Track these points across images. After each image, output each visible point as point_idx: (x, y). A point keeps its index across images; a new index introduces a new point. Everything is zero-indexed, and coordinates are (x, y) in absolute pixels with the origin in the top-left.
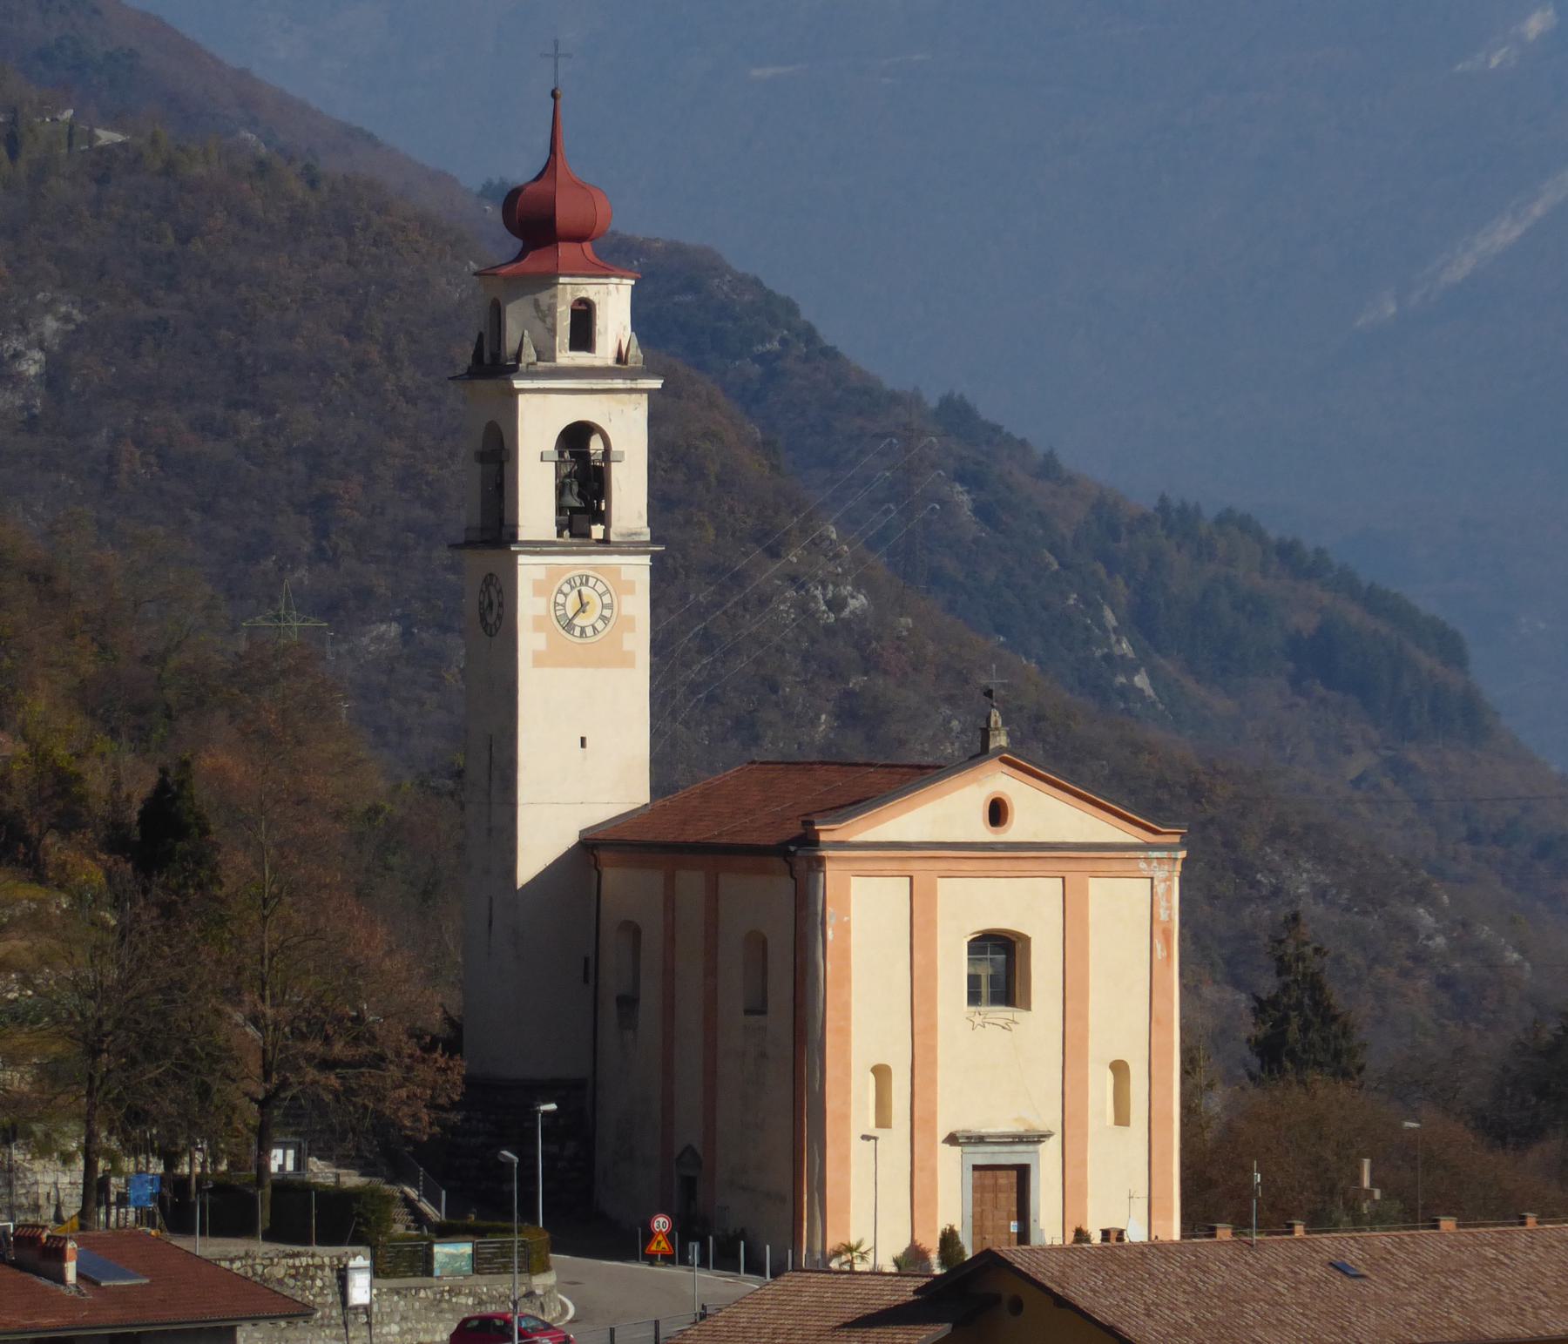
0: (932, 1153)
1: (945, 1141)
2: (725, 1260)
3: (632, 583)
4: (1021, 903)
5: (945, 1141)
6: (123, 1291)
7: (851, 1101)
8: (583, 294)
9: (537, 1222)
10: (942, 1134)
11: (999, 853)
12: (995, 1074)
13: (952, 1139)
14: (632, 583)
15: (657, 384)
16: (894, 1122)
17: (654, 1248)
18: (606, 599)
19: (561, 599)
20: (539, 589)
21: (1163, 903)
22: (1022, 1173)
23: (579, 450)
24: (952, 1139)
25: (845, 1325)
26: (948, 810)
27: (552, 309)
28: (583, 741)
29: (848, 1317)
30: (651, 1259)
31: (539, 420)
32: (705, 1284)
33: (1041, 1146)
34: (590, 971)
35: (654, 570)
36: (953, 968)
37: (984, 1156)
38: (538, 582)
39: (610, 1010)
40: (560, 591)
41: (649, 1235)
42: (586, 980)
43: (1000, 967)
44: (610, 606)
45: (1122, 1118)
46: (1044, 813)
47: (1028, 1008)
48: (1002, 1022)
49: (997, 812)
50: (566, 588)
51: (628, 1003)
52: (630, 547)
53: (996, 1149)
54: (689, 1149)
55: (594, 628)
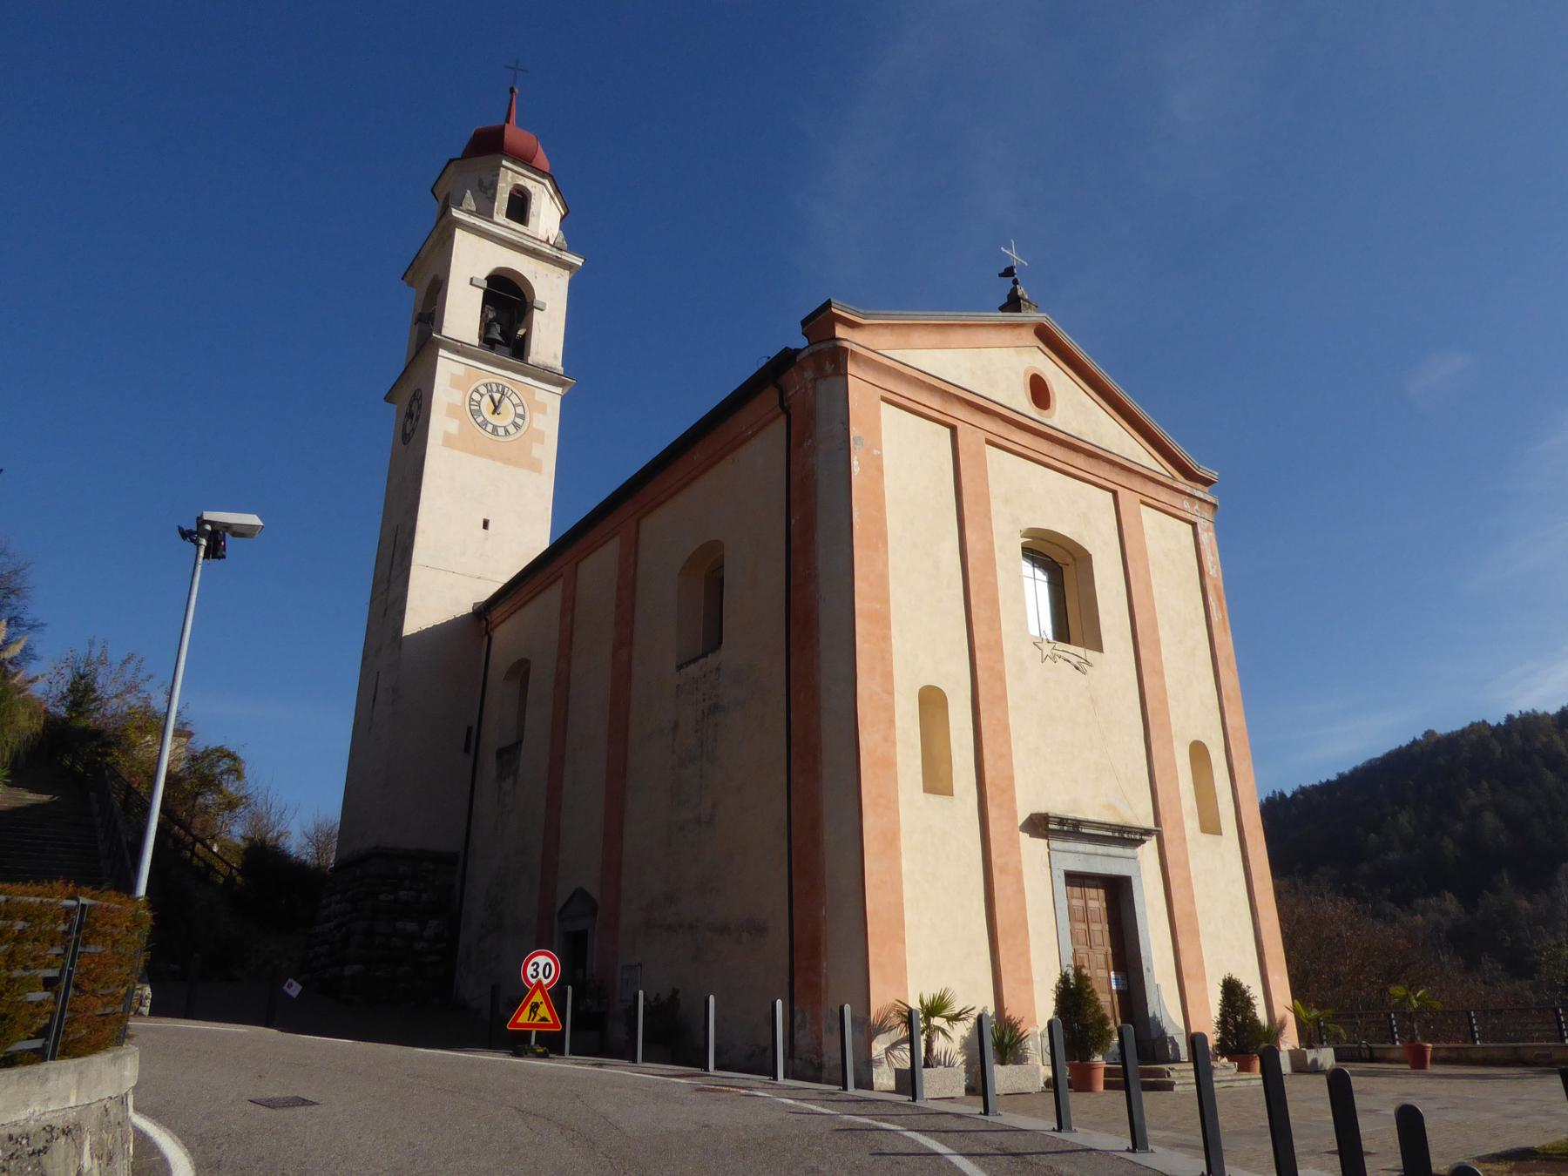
2: (674, 1042)
3: (545, 406)
6: (786, 1105)
7: (890, 741)
8: (523, 182)
9: (131, 887)
10: (1022, 817)
12: (1074, 739)
13: (1039, 825)
14: (545, 406)
15: (579, 261)
17: (523, 1019)
18: (520, 410)
19: (476, 397)
20: (456, 382)
23: (507, 301)
24: (1039, 825)
25: (314, 1104)
27: (493, 186)
28: (486, 525)
29: (311, 1109)
30: (517, 1044)
31: (472, 259)
32: (633, 1091)
33: (1139, 849)
34: (472, 740)
35: (571, 283)
38: (454, 381)
39: (490, 764)
40: (477, 390)
41: (518, 994)
42: (467, 750)
44: (522, 417)
50: (483, 390)
51: (509, 754)
52: (543, 374)
54: (580, 894)
55: (507, 431)
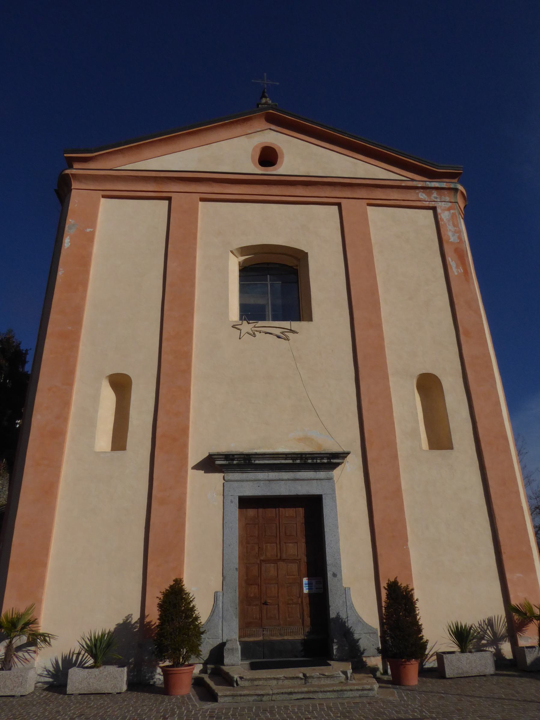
0: (180, 480)
1: (197, 467)
4: (305, 229)
5: (197, 467)
10: (195, 455)
11: (266, 182)
13: (209, 464)
16: (254, 672)
21: (450, 227)
22: (312, 509)
24: (209, 464)
26: (232, 151)
33: (336, 472)
36: (220, 287)
37: (255, 484)
43: (276, 284)
45: (439, 437)
46: (301, 156)
47: (310, 319)
48: (278, 332)
49: (268, 157)
53: (273, 475)
